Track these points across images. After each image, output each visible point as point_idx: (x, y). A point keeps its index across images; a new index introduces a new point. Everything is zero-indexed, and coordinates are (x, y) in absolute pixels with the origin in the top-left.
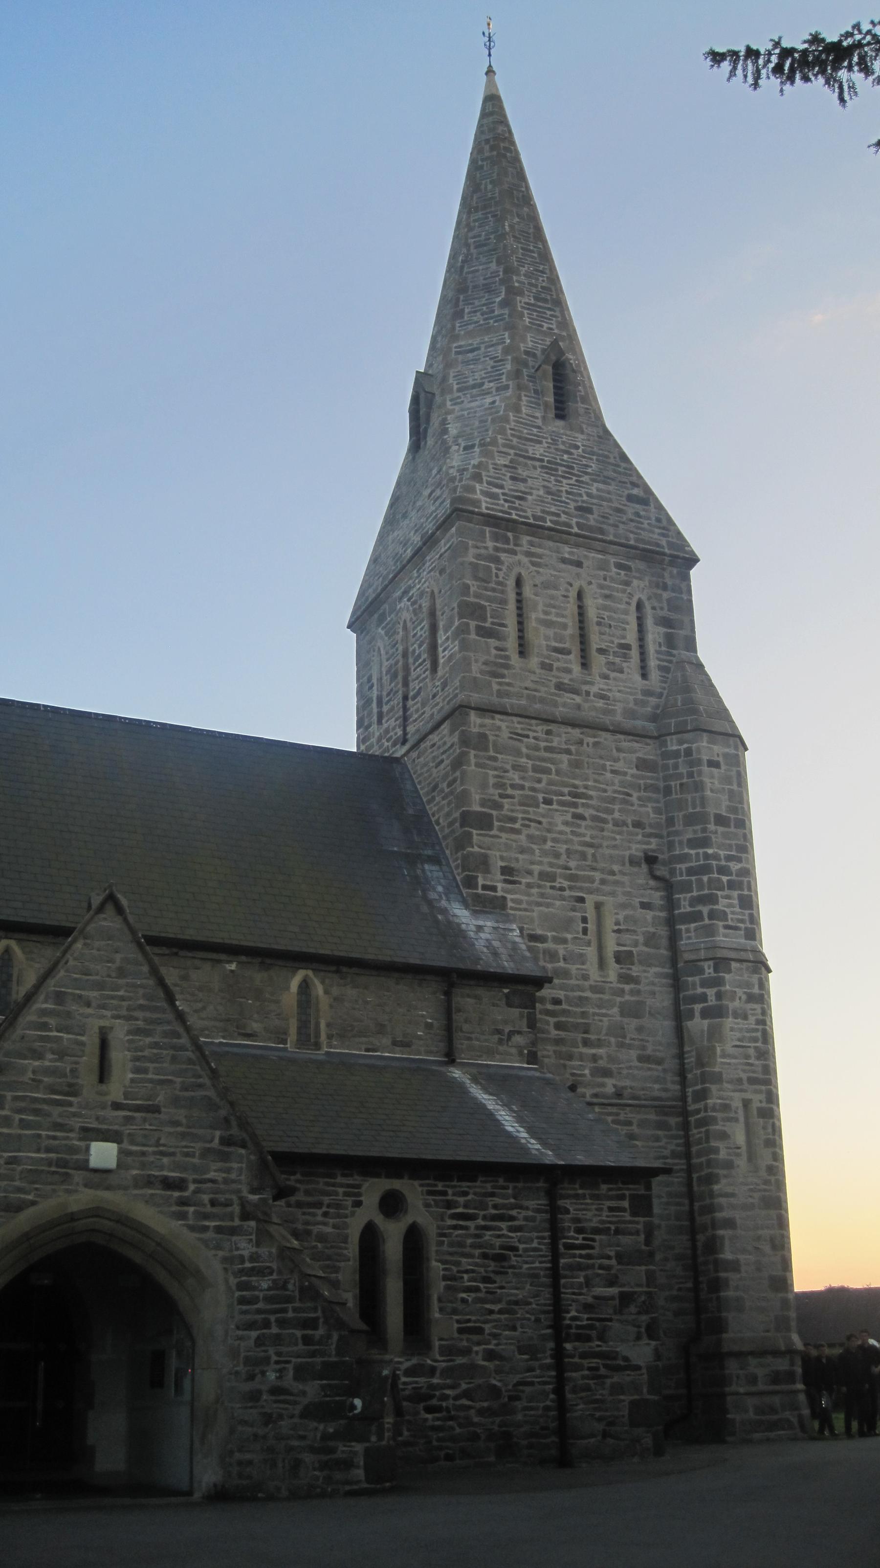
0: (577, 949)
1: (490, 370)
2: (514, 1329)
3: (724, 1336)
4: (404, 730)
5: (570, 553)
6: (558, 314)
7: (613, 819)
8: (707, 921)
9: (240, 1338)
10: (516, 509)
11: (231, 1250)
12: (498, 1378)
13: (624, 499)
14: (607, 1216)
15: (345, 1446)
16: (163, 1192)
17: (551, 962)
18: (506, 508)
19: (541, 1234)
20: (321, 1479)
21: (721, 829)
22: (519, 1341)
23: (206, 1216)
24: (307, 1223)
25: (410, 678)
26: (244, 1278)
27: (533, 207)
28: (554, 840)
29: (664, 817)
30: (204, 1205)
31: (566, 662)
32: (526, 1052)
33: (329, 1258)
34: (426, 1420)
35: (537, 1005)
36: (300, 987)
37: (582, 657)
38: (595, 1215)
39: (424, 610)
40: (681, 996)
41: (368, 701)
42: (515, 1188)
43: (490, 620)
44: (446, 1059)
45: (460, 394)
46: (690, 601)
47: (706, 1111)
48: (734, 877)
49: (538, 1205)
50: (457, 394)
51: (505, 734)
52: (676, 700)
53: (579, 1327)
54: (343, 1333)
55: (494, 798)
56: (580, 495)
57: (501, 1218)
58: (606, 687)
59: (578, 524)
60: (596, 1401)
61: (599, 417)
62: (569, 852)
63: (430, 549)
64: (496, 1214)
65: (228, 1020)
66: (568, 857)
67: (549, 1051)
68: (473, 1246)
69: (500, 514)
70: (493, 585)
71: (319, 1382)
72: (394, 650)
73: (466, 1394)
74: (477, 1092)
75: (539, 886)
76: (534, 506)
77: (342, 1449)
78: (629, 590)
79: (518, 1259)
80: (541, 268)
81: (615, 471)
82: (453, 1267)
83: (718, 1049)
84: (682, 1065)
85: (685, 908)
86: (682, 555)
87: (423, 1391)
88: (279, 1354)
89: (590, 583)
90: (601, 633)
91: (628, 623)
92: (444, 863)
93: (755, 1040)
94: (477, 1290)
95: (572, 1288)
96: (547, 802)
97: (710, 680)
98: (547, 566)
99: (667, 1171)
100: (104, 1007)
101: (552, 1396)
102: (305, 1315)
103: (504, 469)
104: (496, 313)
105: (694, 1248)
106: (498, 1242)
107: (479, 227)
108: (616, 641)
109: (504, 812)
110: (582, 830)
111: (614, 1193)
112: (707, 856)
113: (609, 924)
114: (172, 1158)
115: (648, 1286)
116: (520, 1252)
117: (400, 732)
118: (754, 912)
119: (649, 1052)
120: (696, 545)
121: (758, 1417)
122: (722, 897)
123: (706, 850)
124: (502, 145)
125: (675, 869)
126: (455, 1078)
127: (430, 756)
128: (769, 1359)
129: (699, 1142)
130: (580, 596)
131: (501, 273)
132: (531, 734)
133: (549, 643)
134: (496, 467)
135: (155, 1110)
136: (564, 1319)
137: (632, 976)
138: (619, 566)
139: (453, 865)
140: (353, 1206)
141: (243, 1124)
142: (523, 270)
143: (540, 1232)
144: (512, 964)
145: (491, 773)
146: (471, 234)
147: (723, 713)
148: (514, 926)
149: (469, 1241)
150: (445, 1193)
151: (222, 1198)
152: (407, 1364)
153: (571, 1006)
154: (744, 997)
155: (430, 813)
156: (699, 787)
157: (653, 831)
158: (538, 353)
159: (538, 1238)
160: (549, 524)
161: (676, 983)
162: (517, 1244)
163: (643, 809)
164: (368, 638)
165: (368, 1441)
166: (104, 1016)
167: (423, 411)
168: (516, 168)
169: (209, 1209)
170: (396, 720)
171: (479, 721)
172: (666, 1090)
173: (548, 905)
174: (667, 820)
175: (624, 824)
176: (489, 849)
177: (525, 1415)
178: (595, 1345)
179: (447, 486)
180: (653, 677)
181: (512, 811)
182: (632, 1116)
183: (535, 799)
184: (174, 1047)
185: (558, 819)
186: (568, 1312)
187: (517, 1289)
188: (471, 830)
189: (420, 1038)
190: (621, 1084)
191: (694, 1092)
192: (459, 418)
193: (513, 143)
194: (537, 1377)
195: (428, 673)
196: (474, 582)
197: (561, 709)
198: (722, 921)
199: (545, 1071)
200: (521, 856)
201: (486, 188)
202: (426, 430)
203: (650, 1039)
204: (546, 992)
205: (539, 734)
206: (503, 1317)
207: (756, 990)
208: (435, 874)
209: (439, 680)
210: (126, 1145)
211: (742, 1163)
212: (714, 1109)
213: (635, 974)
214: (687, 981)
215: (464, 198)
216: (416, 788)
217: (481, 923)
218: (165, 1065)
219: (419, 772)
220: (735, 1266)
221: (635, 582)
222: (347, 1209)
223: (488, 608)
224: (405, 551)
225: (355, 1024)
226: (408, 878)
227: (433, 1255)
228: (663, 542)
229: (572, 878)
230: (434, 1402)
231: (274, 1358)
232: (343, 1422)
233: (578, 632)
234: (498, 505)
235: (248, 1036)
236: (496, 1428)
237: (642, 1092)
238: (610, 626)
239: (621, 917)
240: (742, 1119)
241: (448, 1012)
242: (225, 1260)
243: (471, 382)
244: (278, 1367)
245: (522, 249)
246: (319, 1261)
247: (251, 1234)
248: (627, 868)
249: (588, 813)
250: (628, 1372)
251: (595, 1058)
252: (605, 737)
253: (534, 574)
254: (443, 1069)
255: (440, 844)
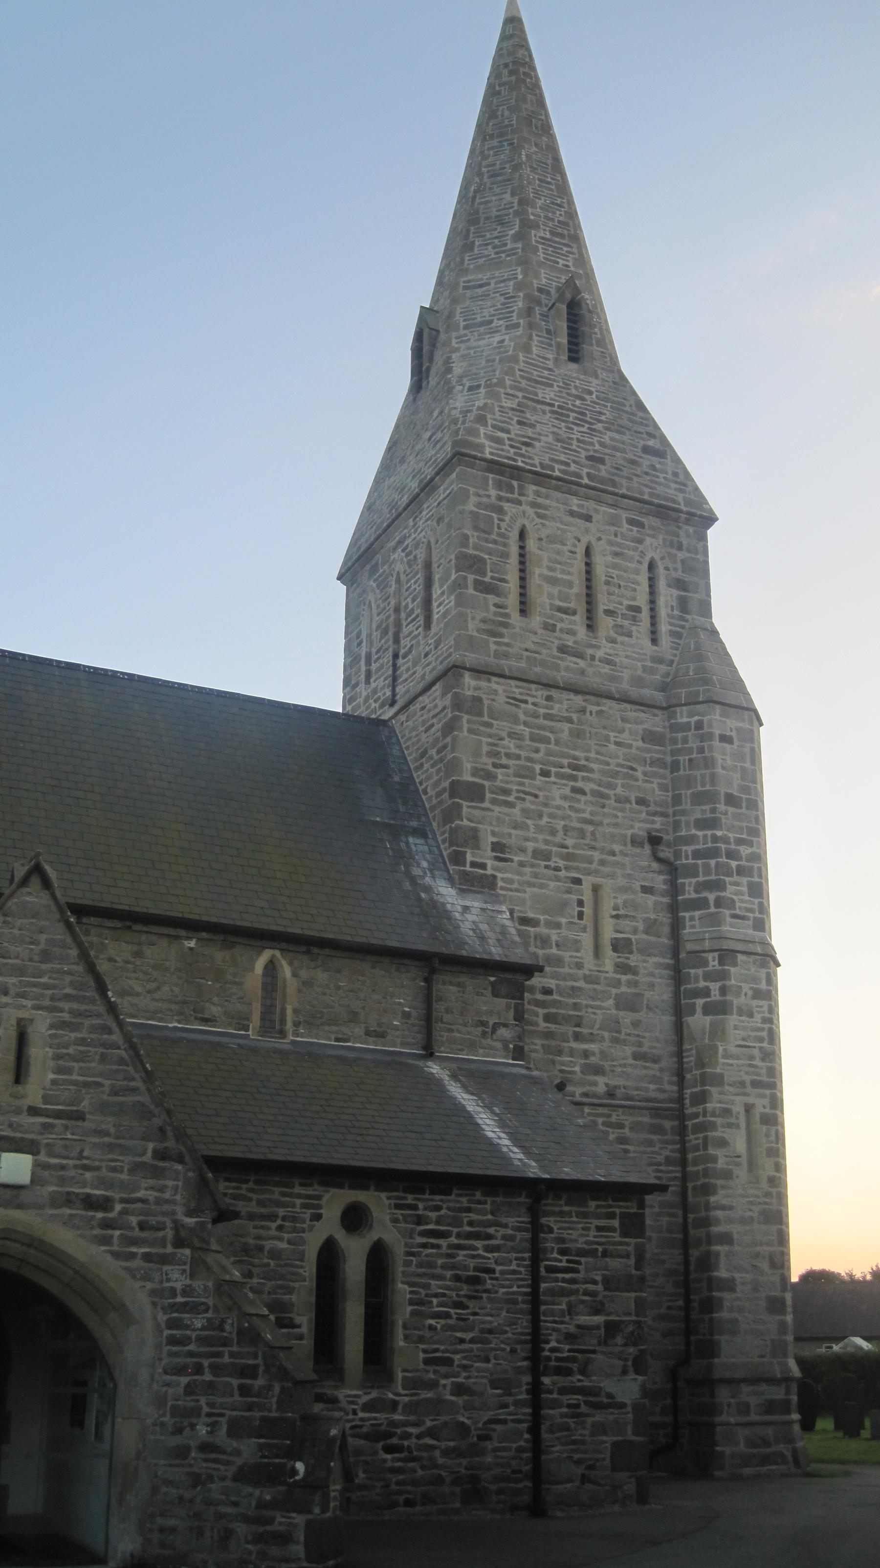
0: (571, 935)
1: (500, 306)
2: (487, 1360)
3: (716, 1360)
4: (394, 691)
5: (579, 506)
6: (575, 250)
7: (615, 795)
8: (713, 910)
9: (168, 1384)
10: (522, 456)
11: (161, 1282)
12: (466, 1415)
13: (639, 450)
14: (595, 1237)
15: (283, 1517)
16: (83, 1213)
17: (543, 948)
18: (511, 455)
19: (520, 1255)
20: (254, 1554)
21: (731, 810)
22: (491, 1374)
23: (134, 1242)
24: (258, 1237)
25: (401, 635)
26: (175, 1315)
27: (552, 137)
28: (551, 816)
29: (670, 794)
30: (130, 1228)
31: (570, 623)
32: (511, 1046)
33: (282, 1277)
34: (385, 1461)
35: (526, 994)
36: (266, 967)
37: (588, 618)
38: (582, 1235)
39: (420, 561)
40: (682, 989)
41: (355, 659)
42: (493, 1203)
43: (489, 574)
44: (424, 1053)
45: (467, 332)
46: (706, 563)
47: (705, 1115)
48: (743, 863)
49: (518, 1222)
50: (462, 332)
51: (502, 698)
52: (688, 668)
53: (558, 1359)
54: (286, 1385)
55: (486, 767)
56: (593, 444)
57: (477, 1236)
58: (612, 652)
59: (588, 474)
60: (574, 1442)
61: (614, 361)
62: (566, 829)
63: (428, 496)
64: (471, 1232)
65: (185, 1002)
66: (565, 835)
67: (536, 1045)
68: (444, 1267)
69: (506, 461)
70: (494, 537)
71: (256, 1440)
72: (386, 604)
73: (432, 1433)
74: (455, 1090)
75: (533, 866)
76: (542, 454)
77: (280, 1521)
78: (641, 548)
79: (495, 1282)
80: (559, 201)
81: (630, 420)
82: (421, 1290)
83: (721, 1049)
84: (680, 1063)
85: (690, 894)
86: (699, 513)
87: (383, 1428)
88: (211, 1405)
89: (599, 539)
90: (609, 594)
91: (638, 584)
92: (430, 836)
93: (761, 1040)
94: (447, 1316)
95: (553, 1316)
96: (545, 774)
97: (724, 648)
98: (553, 518)
99: (663, 1188)
100: (23, 995)
101: (527, 1436)
102: (243, 1361)
103: (511, 413)
104: (509, 247)
105: (686, 1263)
106: (472, 1263)
107: (494, 156)
108: (626, 602)
109: (498, 783)
110: (581, 806)
111: (604, 1210)
112: (715, 839)
113: (607, 909)
114: (96, 1173)
115: (637, 1315)
116: (497, 1275)
117: (388, 693)
118: (764, 901)
119: (644, 1049)
120: (715, 499)
121: (750, 1450)
122: (730, 884)
123: (715, 832)
124: (522, 69)
125: (681, 850)
126: (432, 1074)
127: (420, 720)
128: (764, 1387)
129: (696, 1148)
130: (588, 552)
131: (516, 205)
132: (530, 700)
133: (553, 602)
134: (502, 410)
135: (79, 1116)
136: (544, 1349)
137: (630, 967)
138: (631, 522)
139: (440, 839)
140: (311, 1220)
141: (181, 1136)
142: (539, 203)
143: (518, 1253)
144: (500, 950)
145: (485, 740)
146: (484, 163)
147: (738, 685)
148: (504, 908)
149: (440, 1262)
150: (414, 1207)
151: (153, 1221)
152: (365, 1399)
153: (564, 997)
154: (750, 993)
155: (417, 781)
156: (709, 763)
157: (659, 809)
158: (553, 291)
159: (516, 1259)
160: (557, 473)
161: (678, 976)
162: (493, 1266)
163: (648, 785)
164: (358, 591)
165: (309, 1512)
166: (24, 1006)
167: (426, 348)
168: (535, 95)
169: (137, 1233)
170: (385, 679)
171: (473, 683)
172: (663, 1091)
173: (542, 886)
174: (673, 797)
175: (628, 801)
176: (479, 823)
177: (496, 1457)
178: (576, 1379)
179: (449, 429)
180: (664, 643)
181: (507, 782)
182: (624, 1118)
183: (532, 770)
184: (104, 1045)
185: (556, 793)
186: (548, 1342)
187: (492, 1316)
188: (461, 801)
189: (396, 1028)
190: (613, 1082)
191: (692, 1094)
192: (464, 357)
193: (533, 68)
194: (510, 1414)
195: (421, 629)
196: (476, 534)
197: (563, 673)
198: (729, 909)
199: (532, 1066)
200: (513, 831)
201: (502, 116)
202: (428, 369)
203: (647, 1035)
204: (537, 981)
205: (539, 700)
206: (474, 1346)
207: (763, 986)
208: (421, 848)
209: (432, 638)
210: (43, 1157)
211: (742, 1173)
212: (713, 1114)
213: (633, 964)
214: (689, 973)
215: (479, 126)
216: (403, 752)
217: (467, 903)
218: (93, 1065)
219: (408, 736)
220: (729, 1285)
221: (648, 540)
222: (305, 1223)
223: (488, 561)
224: (401, 498)
225: (325, 1010)
226: (390, 852)
227: (399, 1276)
228: (680, 498)
229: (569, 857)
230: (395, 1441)
231: (206, 1409)
232: (282, 1488)
233: (584, 591)
234: (502, 450)
235: (205, 1021)
236: (463, 1471)
237: (635, 1093)
238: (620, 586)
239: (620, 901)
240: (743, 1125)
241: (428, 1000)
242: (153, 1292)
243: (479, 320)
244: (209, 1420)
245: (540, 180)
246: (270, 1280)
247: (185, 1264)
248: (629, 849)
249: (588, 787)
250: (611, 1410)
251: (586, 1054)
252: (609, 706)
253: (540, 526)
254: (420, 1063)
255: (426, 815)
